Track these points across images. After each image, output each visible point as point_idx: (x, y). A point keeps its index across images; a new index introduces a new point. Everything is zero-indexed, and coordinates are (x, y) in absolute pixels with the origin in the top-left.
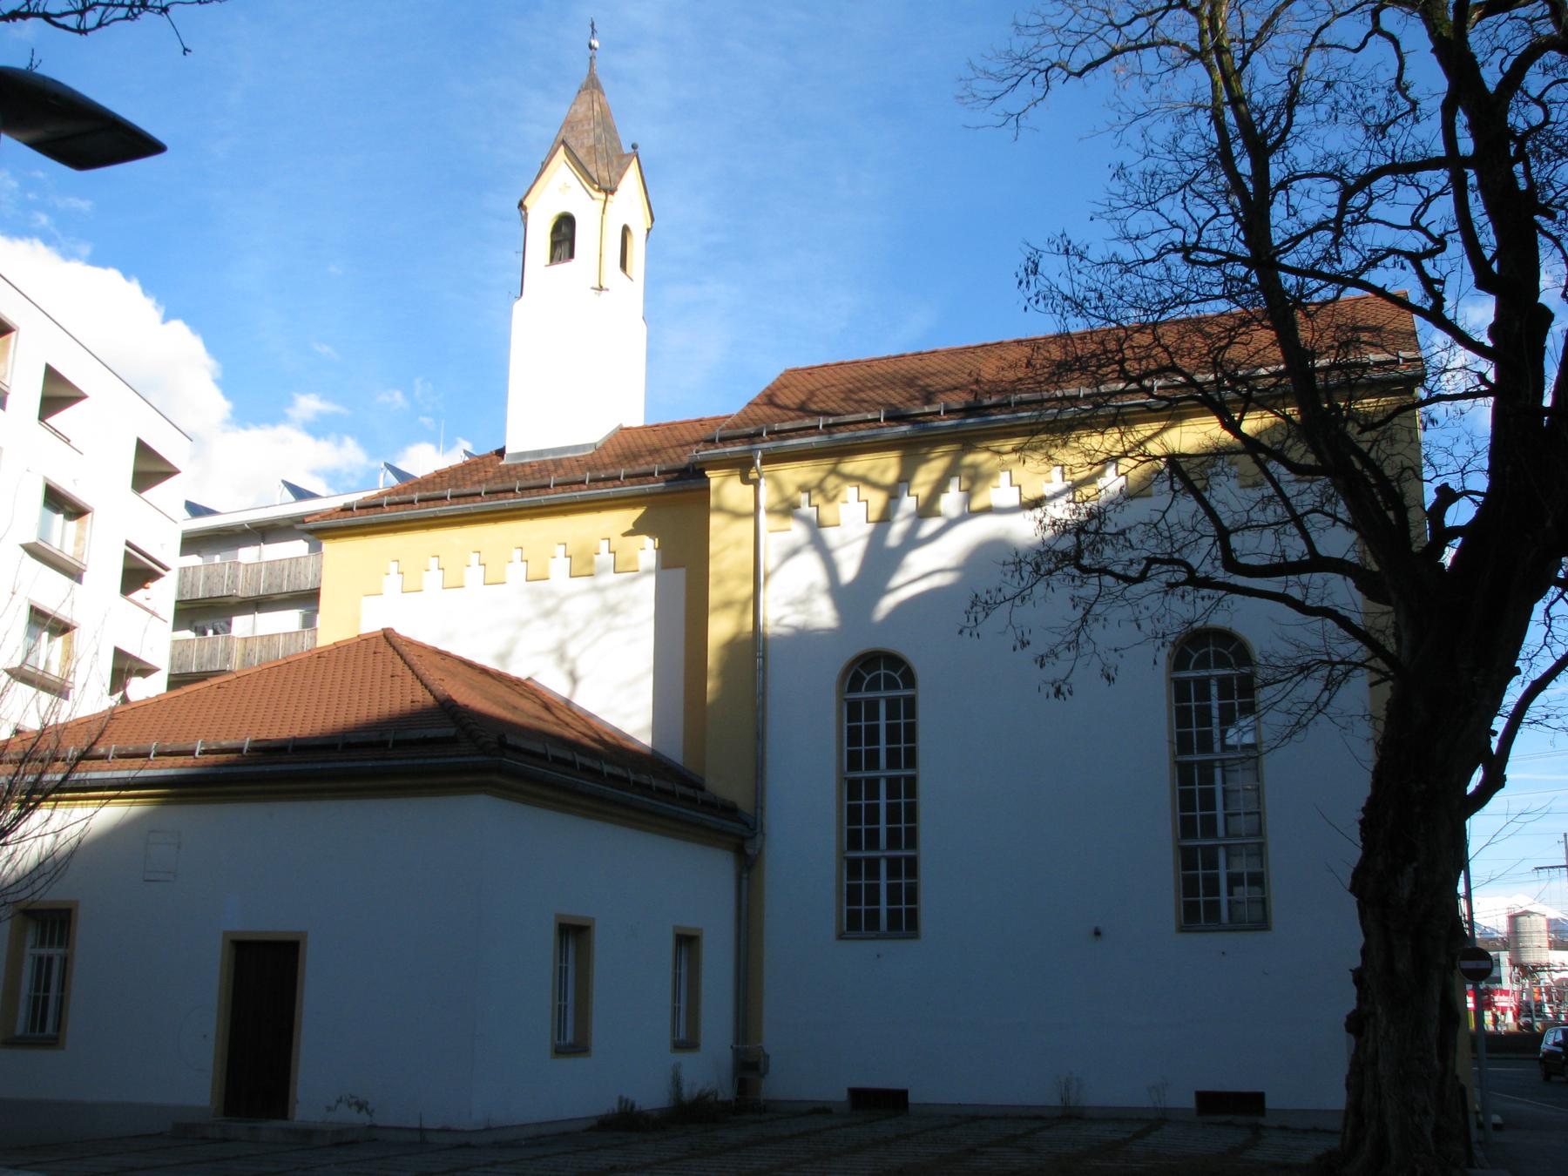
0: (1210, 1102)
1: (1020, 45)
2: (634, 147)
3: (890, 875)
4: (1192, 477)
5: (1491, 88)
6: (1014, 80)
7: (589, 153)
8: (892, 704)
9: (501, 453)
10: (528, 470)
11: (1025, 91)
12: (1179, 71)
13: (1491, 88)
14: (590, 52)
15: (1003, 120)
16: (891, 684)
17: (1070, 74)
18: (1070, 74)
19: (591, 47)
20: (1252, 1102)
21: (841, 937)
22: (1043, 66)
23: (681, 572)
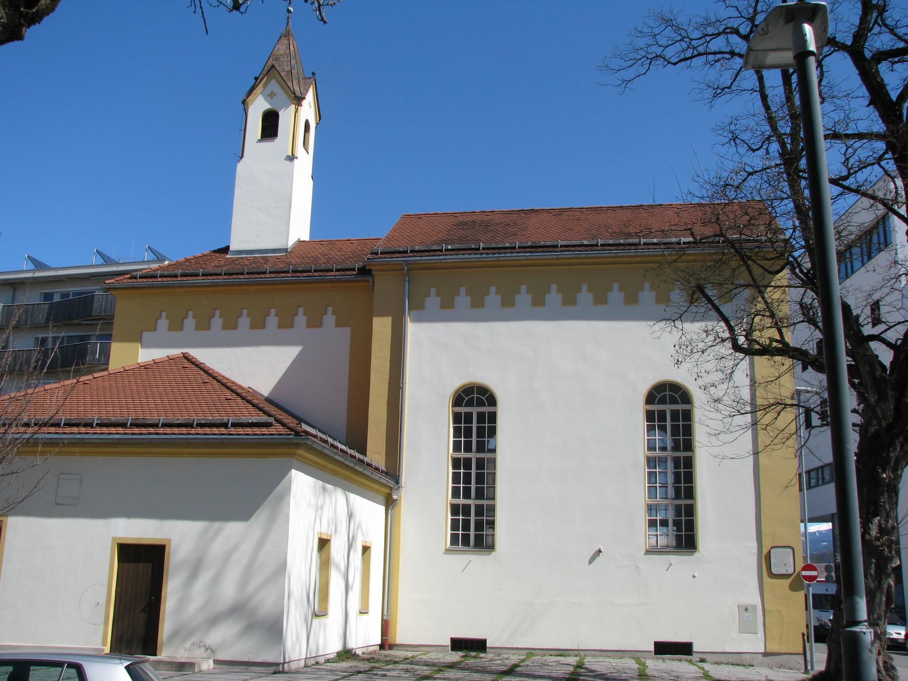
0: (458, 644)
1: (641, 42)
2: (313, 74)
3: (477, 514)
4: (713, 299)
5: (894, 99)
6: (632, 62)
7: (287, 75)
8: (481, 417)
9: (226, 250)
10: (247, 262)
11: (639, 69)
12: (658, 71)
13: (894, 99)
14: (287, 14)
15: (620, 82)
16: (480, 403)
17: (669, 63)
18: (669, 63)
19: (289, 11)
20: (479, 645)
21: (447, 551)
22: (650, 56)
23: (347, 331)
